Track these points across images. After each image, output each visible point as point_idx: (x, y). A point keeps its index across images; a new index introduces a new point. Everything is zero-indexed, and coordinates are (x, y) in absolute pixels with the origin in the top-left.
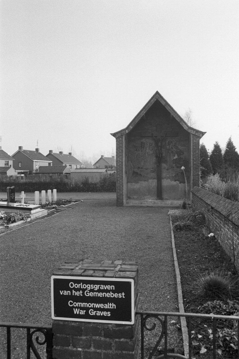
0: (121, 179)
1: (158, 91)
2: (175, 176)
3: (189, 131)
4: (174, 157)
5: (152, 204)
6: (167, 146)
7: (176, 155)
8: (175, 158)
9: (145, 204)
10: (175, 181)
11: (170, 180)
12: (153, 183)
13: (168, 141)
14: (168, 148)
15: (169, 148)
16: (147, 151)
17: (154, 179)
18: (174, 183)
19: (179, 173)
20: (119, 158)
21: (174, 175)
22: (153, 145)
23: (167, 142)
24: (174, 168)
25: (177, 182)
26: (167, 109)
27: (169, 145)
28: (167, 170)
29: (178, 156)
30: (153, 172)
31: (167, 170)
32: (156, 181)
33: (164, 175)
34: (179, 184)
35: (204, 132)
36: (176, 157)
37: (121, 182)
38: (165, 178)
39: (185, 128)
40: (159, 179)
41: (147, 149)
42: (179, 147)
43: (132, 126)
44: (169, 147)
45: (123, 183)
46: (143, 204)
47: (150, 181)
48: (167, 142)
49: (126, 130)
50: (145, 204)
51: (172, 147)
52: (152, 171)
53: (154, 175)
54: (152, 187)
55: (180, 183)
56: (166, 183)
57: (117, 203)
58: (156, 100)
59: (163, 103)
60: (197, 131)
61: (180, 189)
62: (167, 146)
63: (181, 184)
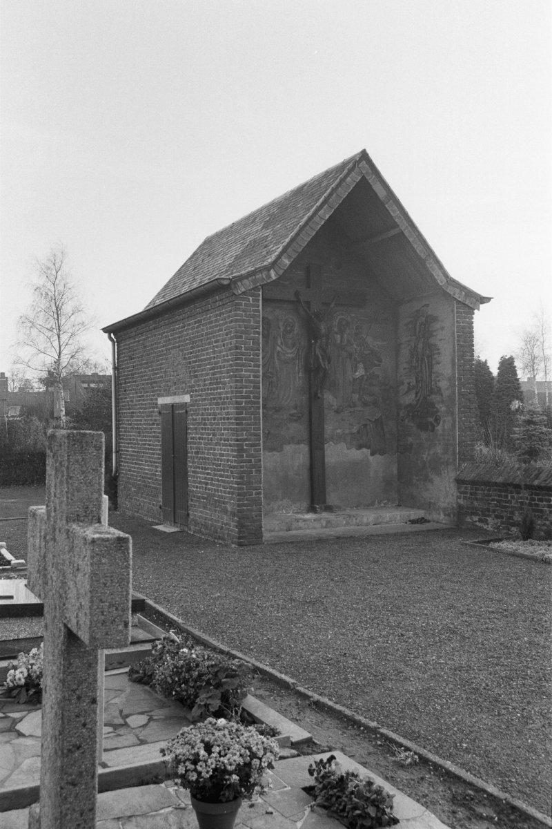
0: (251, 445)
1: (368, 151)
2: (358, 432)
3: (450, 290)
4: (355, 371)
5: (322, 527)
6: (335, 335)
7: (361, 366)
8: (358, 374)
9: (300, 528)
10: (360, 447)
11: (344, 445)
12: (296, 456)
13: (337, 321)
14: (339, 342)
15: (341, 341)
16: (278, 348)
17: (298, 443)
18: (356, 454)
19: (368, 422)
20: (246, 371)
21: (355, 430)
22: (296, 330)
23: (336, 323)
24: (355, 406)
25: (365, 450)
26: (392, 214)
27: (341, 332)
28: (337, 412)
29: (366, 369)
30: (296, 421)
31: (337, 412)
32: (305, 448)
33: (329, 428)
34: (371, 458)
35: (486, 298)
36: (360, 372)
37: (252, 456)
38: (332, 438)
39: (441, 280)
40: (315, 443)
41: (279, 342)
42: (369, 340)
43: (289, 257)
44: (342, 337)
45: (260, 461)
46: (297, 529)
47: (288, 448)
48: (336, 323)
49: (269, 270)
50: (300, 528)
51: (348, 341)
52: (292, 415)
53: (298, 429)
54: (296, 468)
55: (372, 454)
56: (337, 454)
57: (240, 532)
58: (360, 178)
59: (381, 193)
60: (469, 293)
61: (372, 474)
62: (335, 335)
63: (372, 457)
